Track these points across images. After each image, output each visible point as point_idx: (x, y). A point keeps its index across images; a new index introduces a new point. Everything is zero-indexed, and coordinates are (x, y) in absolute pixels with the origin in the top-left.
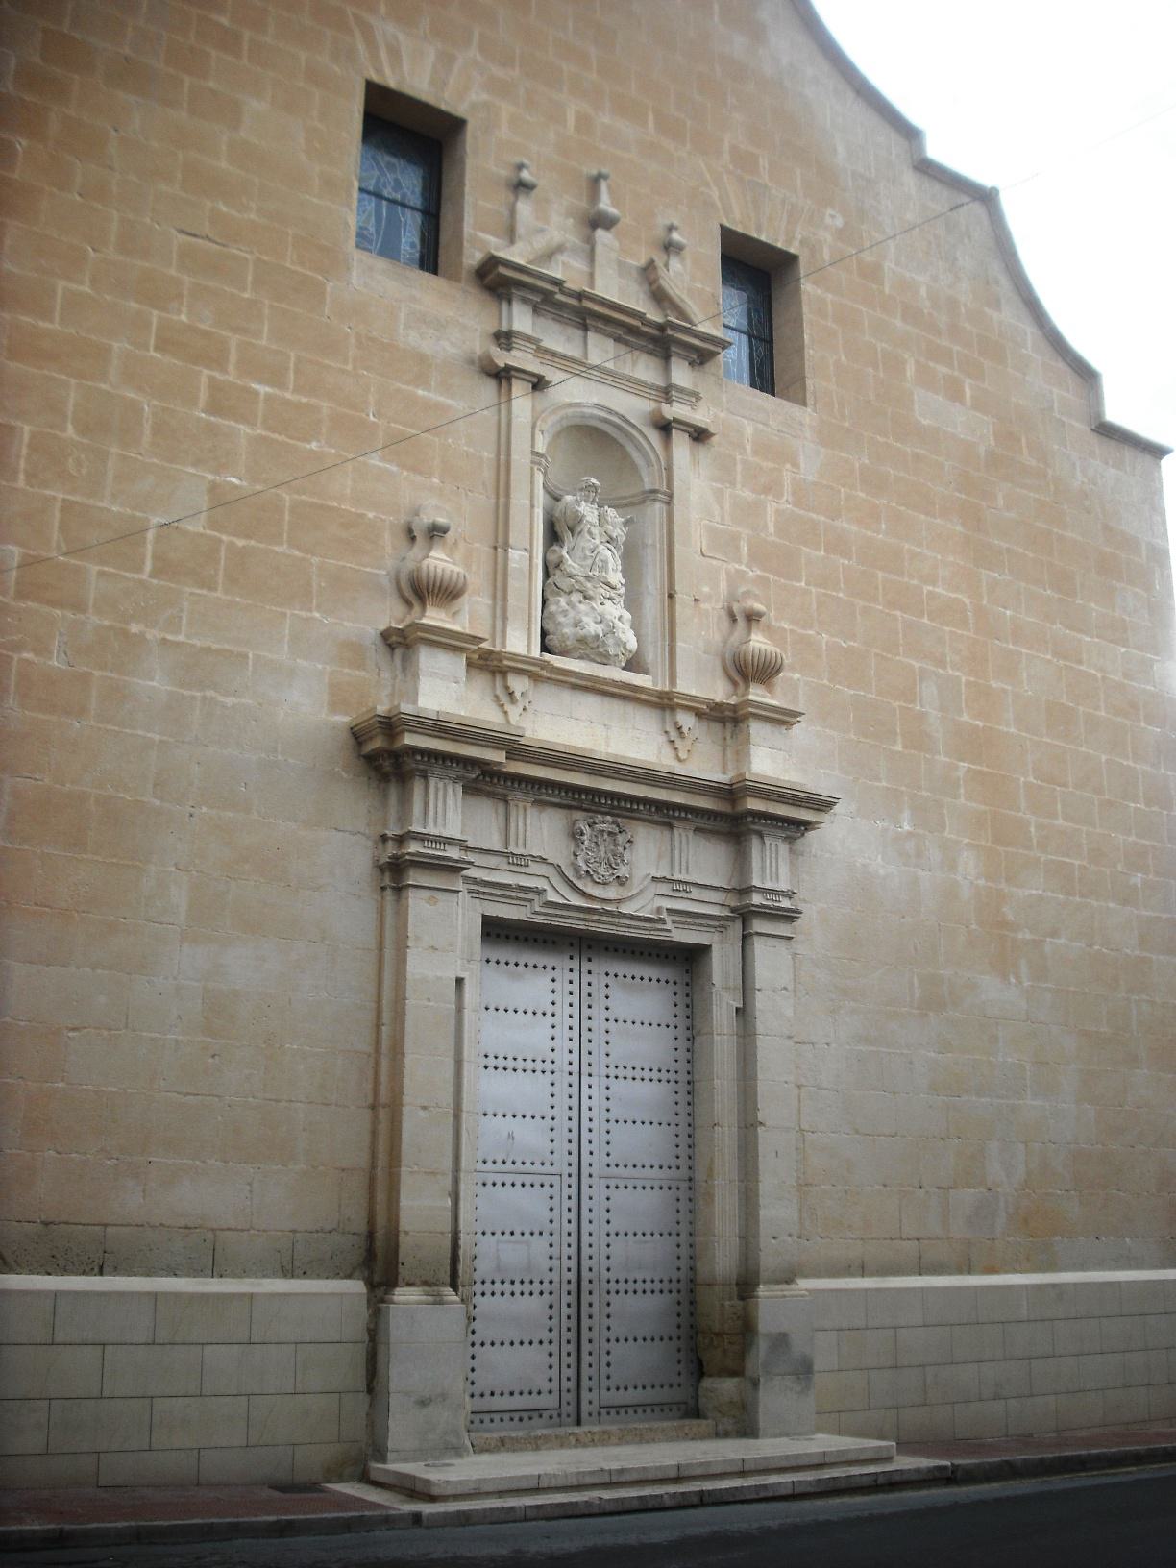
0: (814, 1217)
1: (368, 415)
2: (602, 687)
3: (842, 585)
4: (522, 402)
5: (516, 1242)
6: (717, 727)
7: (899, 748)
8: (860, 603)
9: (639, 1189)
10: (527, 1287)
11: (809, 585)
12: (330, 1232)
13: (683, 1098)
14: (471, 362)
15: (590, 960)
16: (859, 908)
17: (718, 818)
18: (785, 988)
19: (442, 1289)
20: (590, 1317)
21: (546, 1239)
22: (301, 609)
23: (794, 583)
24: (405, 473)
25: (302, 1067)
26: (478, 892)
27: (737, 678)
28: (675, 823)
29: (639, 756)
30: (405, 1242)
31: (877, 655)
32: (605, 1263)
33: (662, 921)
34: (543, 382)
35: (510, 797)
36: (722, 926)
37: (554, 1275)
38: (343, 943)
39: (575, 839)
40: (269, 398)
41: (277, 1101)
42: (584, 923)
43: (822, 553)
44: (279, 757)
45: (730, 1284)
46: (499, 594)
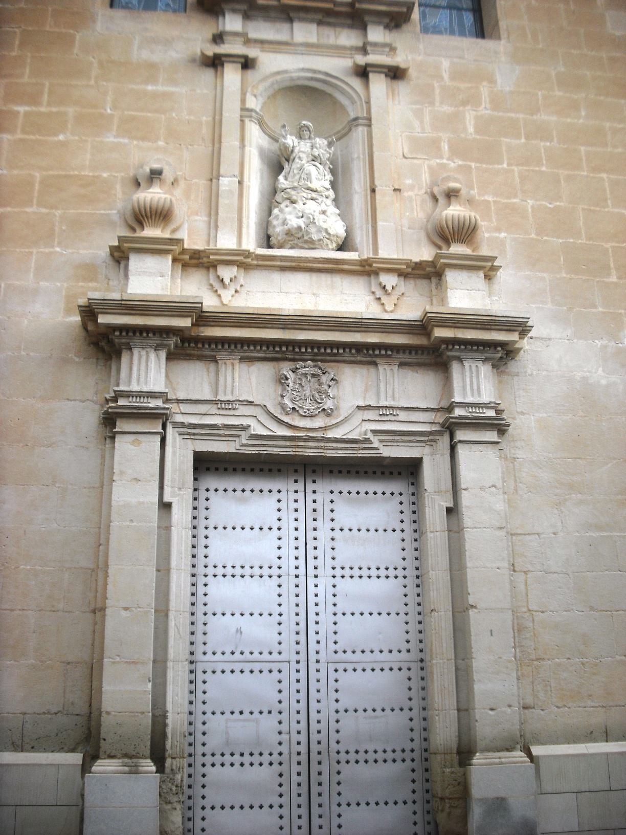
0: (549, 688)
1: (106, 110)
2: (305, 265)
3: (544, 162)
4: (232, 75)
5: (245, 720)
6: (424, 283)
7: (614, 279)
8: (563, 173)
9: (369, 671)
10: (256, 759)
11: (512, 165)
12: (56, 714)
13: (412, 590)
14: (193, 61)
15: (314, 482)
16: (582, 414)
17: (420, 352)
18: (494, 486)
19: (141, 761)
20: (320, 784)
21: (275, 717)
22: (45, 248)
23: (496, 166)
24: (135, 142)
25: (33, 583)
26: (189, 434)
27: (440, 243)
28: (378, 360)
29: (342, 310)
30: (107, 721)
31: (583, 209)
32: (334, 736)
33: (367, 440)
34: (249, 62)
35: (218, 357)
36: (432, 441)
37: (284, 749)
38: (72, 484)
39: (282, 384)
40: (27, 114)
41: (12, 610)
42: (291, 449)
43: (523, 140)
44: (23, 353)
45: (451, 753)
46: (213, 213)
